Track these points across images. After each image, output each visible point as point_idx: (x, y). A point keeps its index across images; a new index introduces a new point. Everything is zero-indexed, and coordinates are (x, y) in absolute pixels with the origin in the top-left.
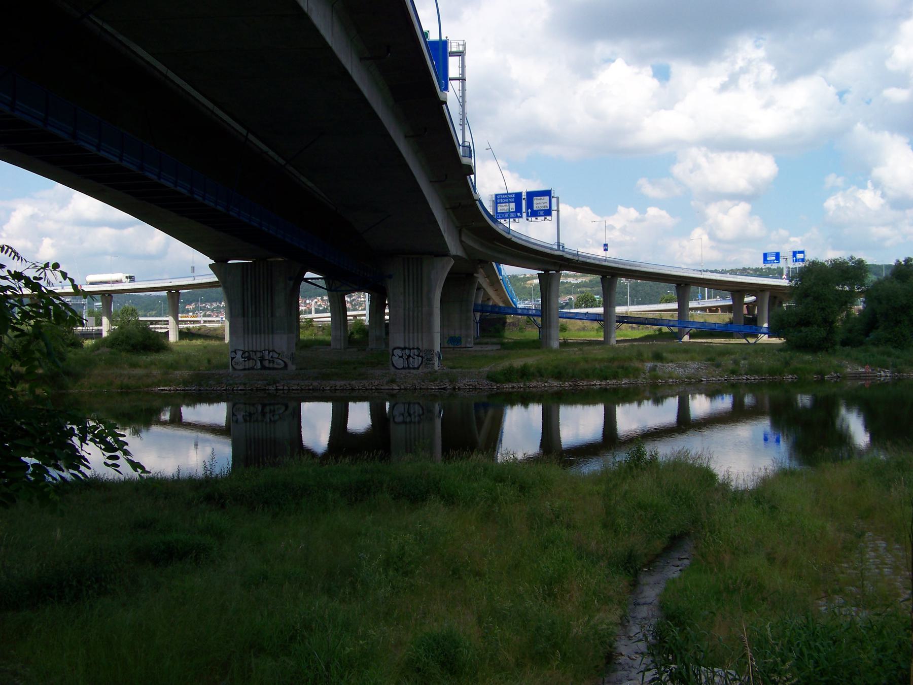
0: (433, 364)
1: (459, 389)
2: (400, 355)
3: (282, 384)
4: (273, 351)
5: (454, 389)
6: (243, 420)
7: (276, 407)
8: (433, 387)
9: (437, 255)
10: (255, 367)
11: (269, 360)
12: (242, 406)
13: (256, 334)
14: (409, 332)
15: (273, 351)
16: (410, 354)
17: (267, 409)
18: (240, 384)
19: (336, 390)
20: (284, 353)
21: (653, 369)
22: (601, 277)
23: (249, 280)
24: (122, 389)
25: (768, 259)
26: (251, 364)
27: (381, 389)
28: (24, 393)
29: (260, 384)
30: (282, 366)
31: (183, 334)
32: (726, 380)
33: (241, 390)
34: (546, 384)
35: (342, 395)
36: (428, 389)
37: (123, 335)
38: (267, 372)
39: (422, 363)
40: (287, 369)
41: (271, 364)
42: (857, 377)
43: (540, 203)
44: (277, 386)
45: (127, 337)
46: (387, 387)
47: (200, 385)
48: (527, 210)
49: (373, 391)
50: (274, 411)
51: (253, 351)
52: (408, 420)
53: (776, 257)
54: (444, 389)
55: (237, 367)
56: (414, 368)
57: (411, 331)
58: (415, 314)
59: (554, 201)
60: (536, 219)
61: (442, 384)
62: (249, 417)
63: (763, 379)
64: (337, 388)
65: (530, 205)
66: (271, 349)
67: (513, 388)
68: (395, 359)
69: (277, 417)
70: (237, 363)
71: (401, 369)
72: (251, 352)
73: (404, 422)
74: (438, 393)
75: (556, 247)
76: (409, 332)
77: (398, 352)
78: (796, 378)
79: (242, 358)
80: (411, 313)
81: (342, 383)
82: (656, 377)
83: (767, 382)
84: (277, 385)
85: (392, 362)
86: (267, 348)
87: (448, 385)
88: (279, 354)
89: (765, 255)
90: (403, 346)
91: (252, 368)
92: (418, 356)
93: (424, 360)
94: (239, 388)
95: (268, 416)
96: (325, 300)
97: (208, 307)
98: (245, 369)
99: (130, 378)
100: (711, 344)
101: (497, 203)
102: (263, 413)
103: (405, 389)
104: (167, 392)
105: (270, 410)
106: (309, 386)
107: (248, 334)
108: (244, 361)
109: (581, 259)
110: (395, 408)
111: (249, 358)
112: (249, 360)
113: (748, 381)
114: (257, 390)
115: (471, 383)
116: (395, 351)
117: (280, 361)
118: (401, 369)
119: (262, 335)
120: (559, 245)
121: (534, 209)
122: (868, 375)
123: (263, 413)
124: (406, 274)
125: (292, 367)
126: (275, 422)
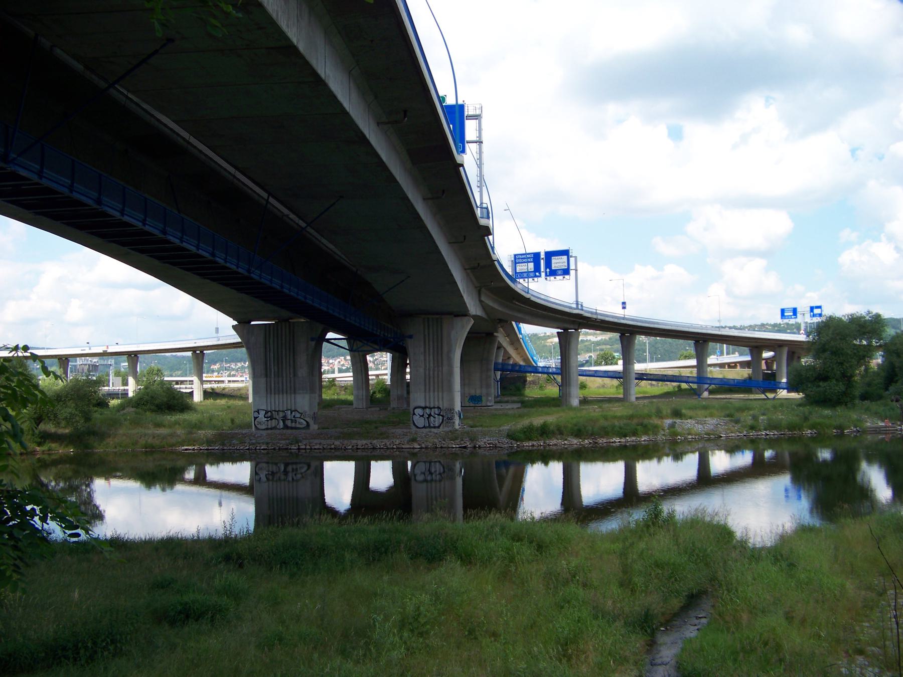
0: (454, 423)
2: (422, 414)
4: (295, 410)
5: (475, 447)
7: (299, 466)
8: (454, 446)
9: (457, 316)
10: (278, 427)
11: (291, 420)
12: (264, 465)
13: (279, 394)
14: (429, 392)
15: (295, 410)
16: (431, 414)
17: (290, 468)
18: (263, 443)
19: (358, 449)
21: (672, 426)
22: (619, 334)
24: (146, 448)
25: (786, 314)
26: (274, 423)
27: (402, 448)
28: (50, 452)
29: (283, 443)
30: (303, 426)
31: (207, 394)
32: (745, 436)
34: (566, 442)
35: (364, 454)
36: (449, 448)
38: (289, 431)
41: (294, 424)
42: (877, 431)
43: (558, 263)
44: (299, 446)
45: (152, 397)
46: (408, 446)
47: (223, 444)
48: (546, 269)
49: (395, 450)
50: (297, 469)
51: (275, 411)
53: (793, 312)
54: (465, 447)
55: (259, 426)
56: (435, 427)
57: (436, 390)
59: (572, 260)
60: (555, 278)
61: (462, 442)
62: (271, 476)
63: (782, 434)
64: (358, 447)
65: (548, 264)
66: (293, 409)
67: (533, 446)
68: (416, 418)
69: (299, 476)
70: (260, 423)
71: (423, 428)
72: (273, 412)
73: (425, 481)
75: (574, 306)
77: (419, 411)
78: (815, 433)
79: (265, 417)
80: (431, 373)
81: (364, 442)
82: (675, 434)
83: (786, 437)
84: (300, 444)
86: (289, 408)
87: (468, 444)
88: (301, 414)
89: (783, 311)
90: (423, 405)
91: (275, 428)
92: (439, 415)
93: (445, 418)
94: (262, 448)
95: (290, 475)
97: (233, 367)
98: (267, 429)
99: (154, 437)
100: (245, 188)
101: (516, 263)
102: (286, 473)
103: (426, 448)
105: (293, 469)
106: (331, 445)
107: (271, 394)
108: (267, 421)
109: (599, 317)
111: (272, 418)
112: (271, 420)
113: (768, 437)
115: (492, 441)
116: (415, 410)
117: (302, 421)
118: (423, 428)
120: (577, 304)
121: (553, 269)
122: (888, 429)
123: (286, 473)
124: (426, 333)
125: (314, 427)
126: (297, 481)
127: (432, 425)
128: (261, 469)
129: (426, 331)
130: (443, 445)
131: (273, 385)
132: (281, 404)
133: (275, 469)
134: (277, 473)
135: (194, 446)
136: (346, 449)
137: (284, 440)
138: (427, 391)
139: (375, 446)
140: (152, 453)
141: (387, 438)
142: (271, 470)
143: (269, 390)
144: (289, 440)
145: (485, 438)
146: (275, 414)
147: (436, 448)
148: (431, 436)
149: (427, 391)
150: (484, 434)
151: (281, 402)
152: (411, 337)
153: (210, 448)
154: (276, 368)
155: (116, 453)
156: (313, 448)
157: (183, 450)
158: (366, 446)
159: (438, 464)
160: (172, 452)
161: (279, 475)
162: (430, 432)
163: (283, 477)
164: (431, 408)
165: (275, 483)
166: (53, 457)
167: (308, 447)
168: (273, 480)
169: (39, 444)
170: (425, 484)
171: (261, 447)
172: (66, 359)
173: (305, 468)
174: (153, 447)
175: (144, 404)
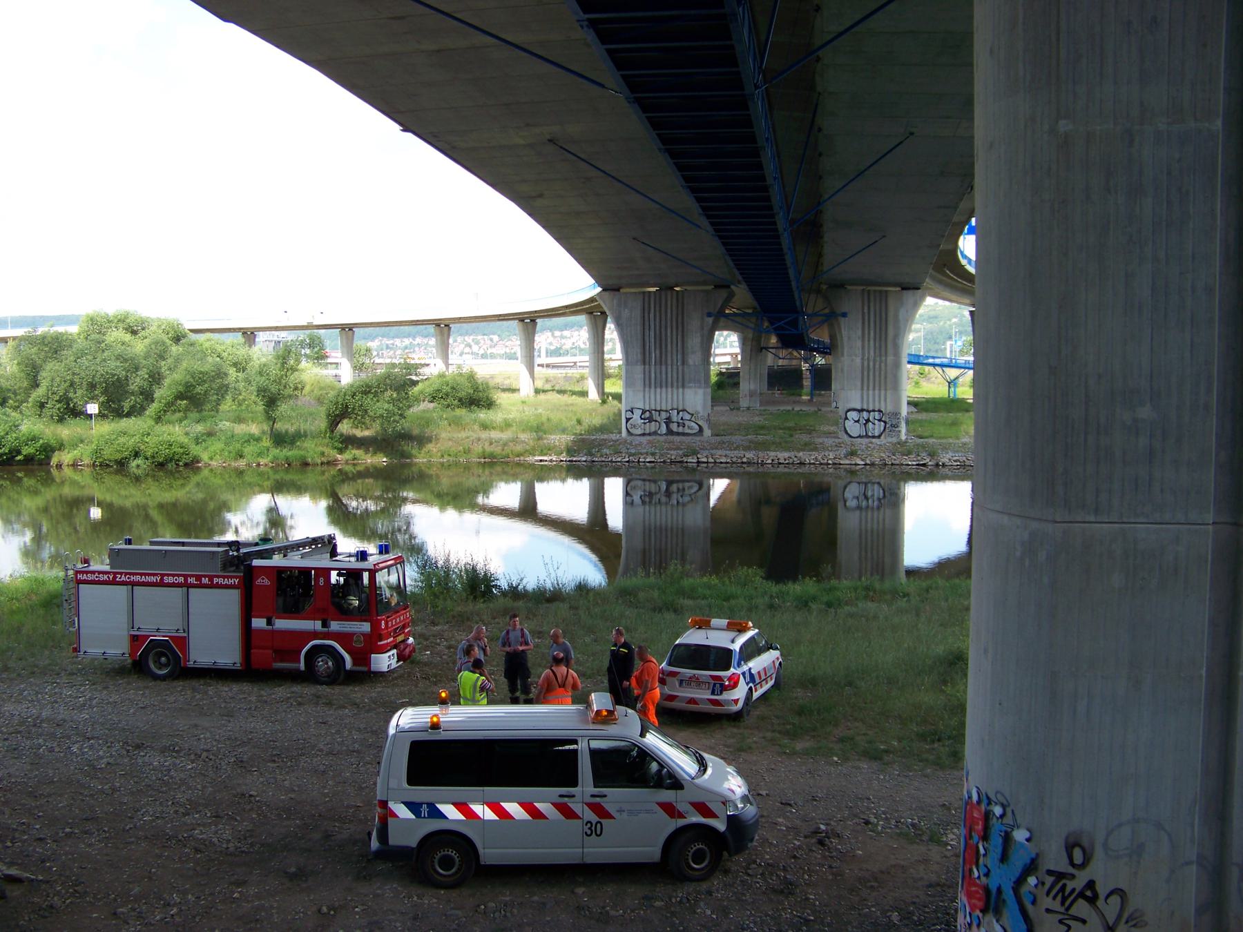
0: (900, 431)
1: (944, 465)
2: (856, 419)
3: (705, 455)
5: (937, 465)
6: (641, 503)
7: (687, 484)
9: (905, 288)
10: (659, 432)
11: (678, 423)
12: (640, 483)
13: (661, 387)
14: (868, 389)
16: (869, 419)
17: (674, 487)
18: (647, 454)
19: (780, 463)
20: (699, 413)
23: (652, 315)
26: (653, 427)
27: (840, 464)
28: (355, 462)
29: (673, 455)
30: (694, 432)
33: (649, 462)
35: (786, 470)
36: (902, 465)
37: (448, 385)
38: (677, 439)
39: (884, 430)
40: (702, 435)
41: (681, 428)
45: (453, 388)
46: (848, 462)
47: (591, 454)
49: (830, 466)
50: (684, 489)
51: (655, 410)
52: (864, 503)
54: (924, 465)
55: (633, 431)
56: (874, 437)
57: (877, 388)
58: (877, 366)
61: (919, 458)
62: (648, 498)
64: (780, 461)
66: (680, 408)
68: (848, 424)
69: (687, 499)
73: (859, 508)
74: (913, 471)
76: (868, 389)
79: (642, 419)
80: (871, 364)
81: (786, 455)
84: (699, 456)
85: (845, 428)
86: (675, 407)
87: (928, 460)
88: (693, 415)
91: (655, 433)
92: (880, 420)
93: (887, 426)
94: (648, 460)
95: (674, 496)
96: (556, 337)
98: (644, 435)
99: (491, 444)
102: (668, 494)
103: (873, 464)
104: (546, 463)
105: (678, 489)
106: (741, 458)
107: (650, 387)
108: (645, 423)
110: (847, 490)
111: (651, 420)
114: (671, 462)
116: (848, 414)
117: (693, 424)
119: (670, 390)
123: (668, 494)
124: (866, 311)
125: (707, 432)
126: (684, 505)
127: (870, 434)
128: (634, 488)
129: (866, 308)
130: (893, 462)
131: (653, 375)
132: (664, 402)
133: (653, 488)
134: (656, 493)
135: (550, 455)
136: (763, 464)
137: (675, 449)
138: (865, 388)
139: (803, 461)
140: (492, 464)
141: (816, 449)
142: (648, 489)
143: (647, 382)
144: (681, 449)
145: (948, 453)
146: (655, 415)
147: (886, 464)
148: (874, 448)
149: (865, 388)
150: (945, 448)
151: (662, 399)
152: (844, 315)
153: (574, 459)
154: (658, 352)
155: (442, 464)
156: (718, 461)
157: (537, 461)
158: (791, 461)
159: (876, 486)
160: (519, 464)
161: (658, 496)
162: (871, 443)
163: (664, 499)
164: (869, 411)
165: (653, 509)
166: (359, 468)
167: (711, 460)
168: (650, 502)
169: (341, 451)
170: (858, 513)
171: (645, 458)
172: (252, 333)
173: (695, 489)
174: (495, 457)
175: (442, 397)
